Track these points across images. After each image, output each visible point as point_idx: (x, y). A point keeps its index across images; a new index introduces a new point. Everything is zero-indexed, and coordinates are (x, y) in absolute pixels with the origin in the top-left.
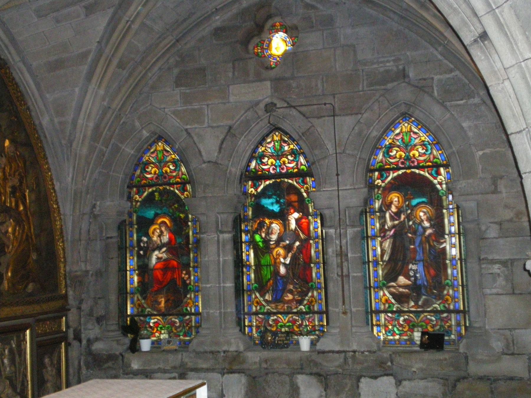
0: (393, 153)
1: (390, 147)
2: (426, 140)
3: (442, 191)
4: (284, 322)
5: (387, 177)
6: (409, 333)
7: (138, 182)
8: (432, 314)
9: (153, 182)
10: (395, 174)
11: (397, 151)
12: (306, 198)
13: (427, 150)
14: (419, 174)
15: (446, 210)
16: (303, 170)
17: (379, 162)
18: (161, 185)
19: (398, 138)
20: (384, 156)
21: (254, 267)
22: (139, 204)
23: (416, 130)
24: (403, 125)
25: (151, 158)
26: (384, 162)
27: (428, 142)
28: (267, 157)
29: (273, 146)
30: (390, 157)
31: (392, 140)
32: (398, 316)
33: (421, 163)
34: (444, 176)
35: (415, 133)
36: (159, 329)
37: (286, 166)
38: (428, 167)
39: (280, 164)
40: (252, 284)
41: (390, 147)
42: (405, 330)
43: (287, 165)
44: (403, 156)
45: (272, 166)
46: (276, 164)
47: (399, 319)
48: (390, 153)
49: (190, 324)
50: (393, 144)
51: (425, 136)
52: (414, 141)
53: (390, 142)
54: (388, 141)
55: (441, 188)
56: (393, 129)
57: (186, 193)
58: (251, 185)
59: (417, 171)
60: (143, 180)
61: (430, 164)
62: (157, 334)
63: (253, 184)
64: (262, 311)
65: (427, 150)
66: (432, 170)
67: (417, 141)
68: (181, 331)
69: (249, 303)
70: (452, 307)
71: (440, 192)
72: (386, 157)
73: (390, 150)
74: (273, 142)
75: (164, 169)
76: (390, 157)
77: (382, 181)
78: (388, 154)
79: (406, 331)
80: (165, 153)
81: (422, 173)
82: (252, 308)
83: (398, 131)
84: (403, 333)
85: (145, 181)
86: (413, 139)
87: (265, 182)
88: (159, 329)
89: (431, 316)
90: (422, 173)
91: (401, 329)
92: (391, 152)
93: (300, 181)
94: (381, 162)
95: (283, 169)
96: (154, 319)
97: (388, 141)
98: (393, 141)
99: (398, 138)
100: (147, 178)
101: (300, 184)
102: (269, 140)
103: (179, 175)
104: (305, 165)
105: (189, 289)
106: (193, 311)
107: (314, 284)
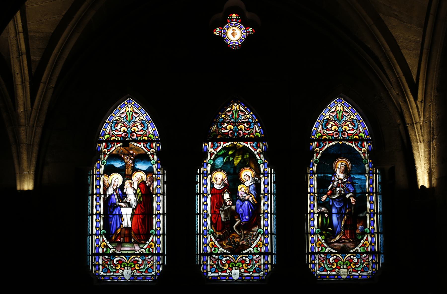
0: (329, 126)
1: (117, 122)
2: (355, 118)
3: (260, 160)
4: (127, 262)
5: (324, 146)
6: (228, 271)
7: (319, 136)
8: (139, 256)
9: (333, 138)
10: (331, 144)
11: (332, 125)
12: (363, 159)
13: (355, 126)
14: (348, 145)
15: (367, 175)
16: (257, 136)
17: (319, 133)
18: (340, 140)
19: (229, 114)
20: (322, 128)
21: (210, 215)
22: (107, 156)
23: (347, 110)
24: (127, 106)
25: (331, 117)
26: (322, 133)
27: (356, 120)
28: (227, 123)
29: (336, 115)
30: (327, 129)
31: (118, 117)
32: (113, 257)
33: (246, 135)
34: (155, 149)
35: (347, 112)
36: (230, 266)
37: (347, 133)
38: (144, 141)
39: (131, 132)
40: (101, 231)
41: (117, 122)
42: (117, 268)
43: (348, 132)
44: (126, 131)
45: (335, 131)
46: (339, 130)
47: (114, 260)
48: (327, 126)
49: (260, 262)
50: (329, 119)
51: (115, 116)
52: (241, 118)
53: (327, 118)
54: (326, 117)
55: (364, 158)
56: (120, 109)
57: (152, 150)
58: (316, 145)
59: (347, 143)
60: (112, 137)
61: (146, 138)
62: (121, 271)
63: (318, 145)
64: (324, 251)
65: (144, 127)
66: (147, 144)
67: (137, 119)
68: (359, 267)
69: (373, 244)
70: (263, 250)
71: (259, 161)
72: (113, 130)
73: (327, 124)
74: (125, 113)
75: (133, 128)
76: (327, 129)
77: (214, 149)
78: (325, 126)
79: (118, 269)
80: (134, 115)
81: (350, 144)
82: (207, 249)
83: (123, 111)
84: (332, 270)
85: (326, 137)
86: (134, 118)
87: (329, 144)
88: (230, 266)
89: (354, 256)
90: (350, 144)
91: (114, 267)
92: (328, 125)
93: (254, 145)
94: (320, 133)
95: (344, 134)
96: (226, 257)
97: (115, 118)
98: (119, 118)
99: (229, 114)
100: (221, 135)
101: (358, 146)
102: (228, 109)
103: (146, 134)
104: (259, 133)
105: (151, 233)
106: (263, 250)
107: (262, 231)
